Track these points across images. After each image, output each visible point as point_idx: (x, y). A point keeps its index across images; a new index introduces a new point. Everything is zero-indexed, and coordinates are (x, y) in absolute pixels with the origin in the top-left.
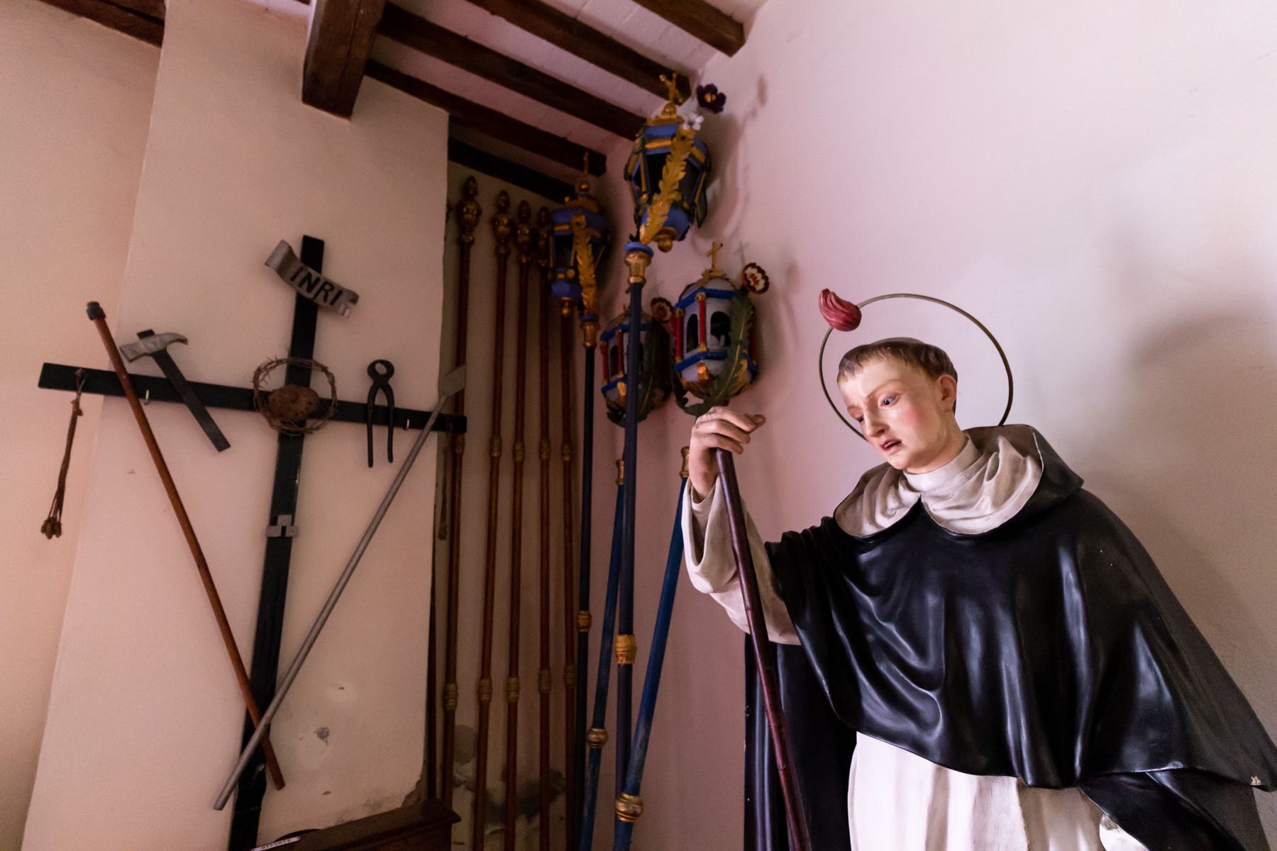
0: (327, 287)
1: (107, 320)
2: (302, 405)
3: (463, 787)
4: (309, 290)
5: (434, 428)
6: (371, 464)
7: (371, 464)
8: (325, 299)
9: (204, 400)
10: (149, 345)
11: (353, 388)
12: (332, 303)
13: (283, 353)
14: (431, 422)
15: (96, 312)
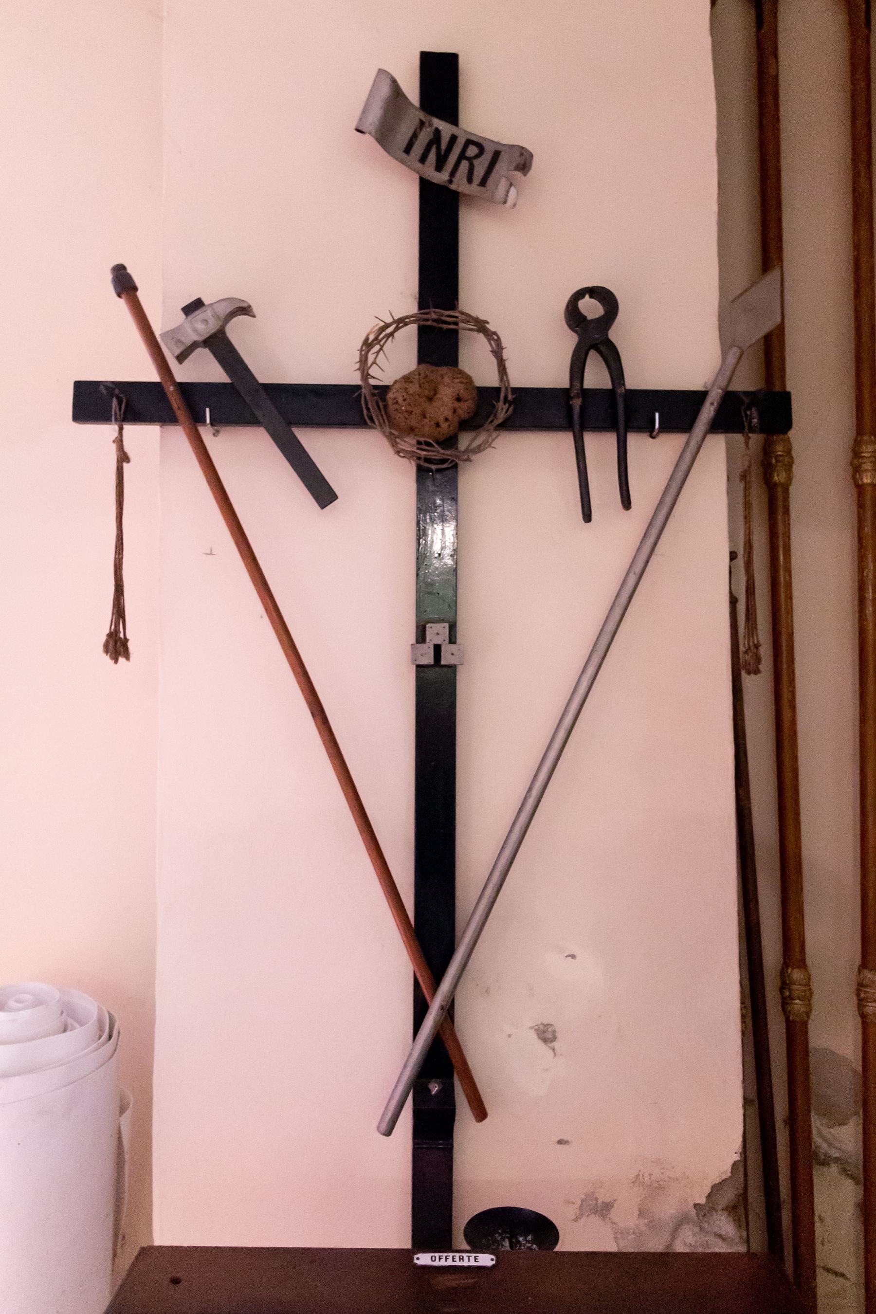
0: (472, 151)
1: (140, 294)
2: (445, 406)
3: (834, 1168)
4: (439, 167)
5: (717, 426)
6: (587, 516)
7: (587, 516)
8: (470, 180)
9: (294, 412)
10: (202, 326)
11: (540, 357)
12: (483, 183)
13: (408, 306)
14: (707, 412)
15: (124, 283)
